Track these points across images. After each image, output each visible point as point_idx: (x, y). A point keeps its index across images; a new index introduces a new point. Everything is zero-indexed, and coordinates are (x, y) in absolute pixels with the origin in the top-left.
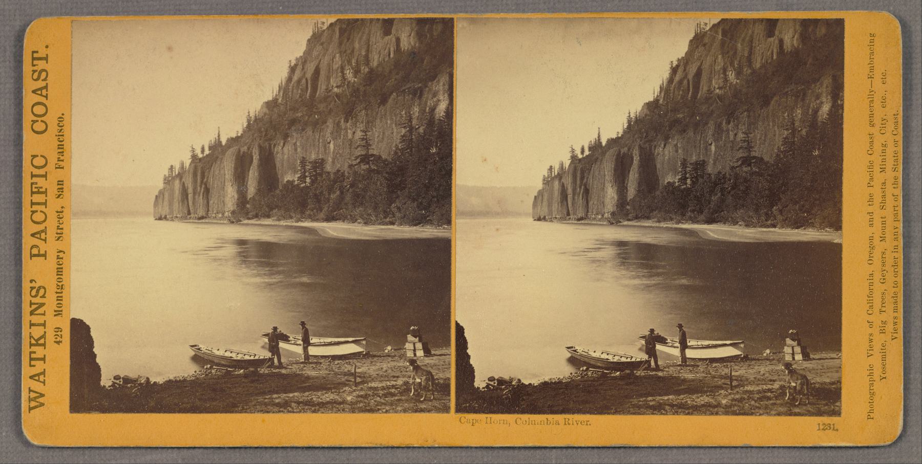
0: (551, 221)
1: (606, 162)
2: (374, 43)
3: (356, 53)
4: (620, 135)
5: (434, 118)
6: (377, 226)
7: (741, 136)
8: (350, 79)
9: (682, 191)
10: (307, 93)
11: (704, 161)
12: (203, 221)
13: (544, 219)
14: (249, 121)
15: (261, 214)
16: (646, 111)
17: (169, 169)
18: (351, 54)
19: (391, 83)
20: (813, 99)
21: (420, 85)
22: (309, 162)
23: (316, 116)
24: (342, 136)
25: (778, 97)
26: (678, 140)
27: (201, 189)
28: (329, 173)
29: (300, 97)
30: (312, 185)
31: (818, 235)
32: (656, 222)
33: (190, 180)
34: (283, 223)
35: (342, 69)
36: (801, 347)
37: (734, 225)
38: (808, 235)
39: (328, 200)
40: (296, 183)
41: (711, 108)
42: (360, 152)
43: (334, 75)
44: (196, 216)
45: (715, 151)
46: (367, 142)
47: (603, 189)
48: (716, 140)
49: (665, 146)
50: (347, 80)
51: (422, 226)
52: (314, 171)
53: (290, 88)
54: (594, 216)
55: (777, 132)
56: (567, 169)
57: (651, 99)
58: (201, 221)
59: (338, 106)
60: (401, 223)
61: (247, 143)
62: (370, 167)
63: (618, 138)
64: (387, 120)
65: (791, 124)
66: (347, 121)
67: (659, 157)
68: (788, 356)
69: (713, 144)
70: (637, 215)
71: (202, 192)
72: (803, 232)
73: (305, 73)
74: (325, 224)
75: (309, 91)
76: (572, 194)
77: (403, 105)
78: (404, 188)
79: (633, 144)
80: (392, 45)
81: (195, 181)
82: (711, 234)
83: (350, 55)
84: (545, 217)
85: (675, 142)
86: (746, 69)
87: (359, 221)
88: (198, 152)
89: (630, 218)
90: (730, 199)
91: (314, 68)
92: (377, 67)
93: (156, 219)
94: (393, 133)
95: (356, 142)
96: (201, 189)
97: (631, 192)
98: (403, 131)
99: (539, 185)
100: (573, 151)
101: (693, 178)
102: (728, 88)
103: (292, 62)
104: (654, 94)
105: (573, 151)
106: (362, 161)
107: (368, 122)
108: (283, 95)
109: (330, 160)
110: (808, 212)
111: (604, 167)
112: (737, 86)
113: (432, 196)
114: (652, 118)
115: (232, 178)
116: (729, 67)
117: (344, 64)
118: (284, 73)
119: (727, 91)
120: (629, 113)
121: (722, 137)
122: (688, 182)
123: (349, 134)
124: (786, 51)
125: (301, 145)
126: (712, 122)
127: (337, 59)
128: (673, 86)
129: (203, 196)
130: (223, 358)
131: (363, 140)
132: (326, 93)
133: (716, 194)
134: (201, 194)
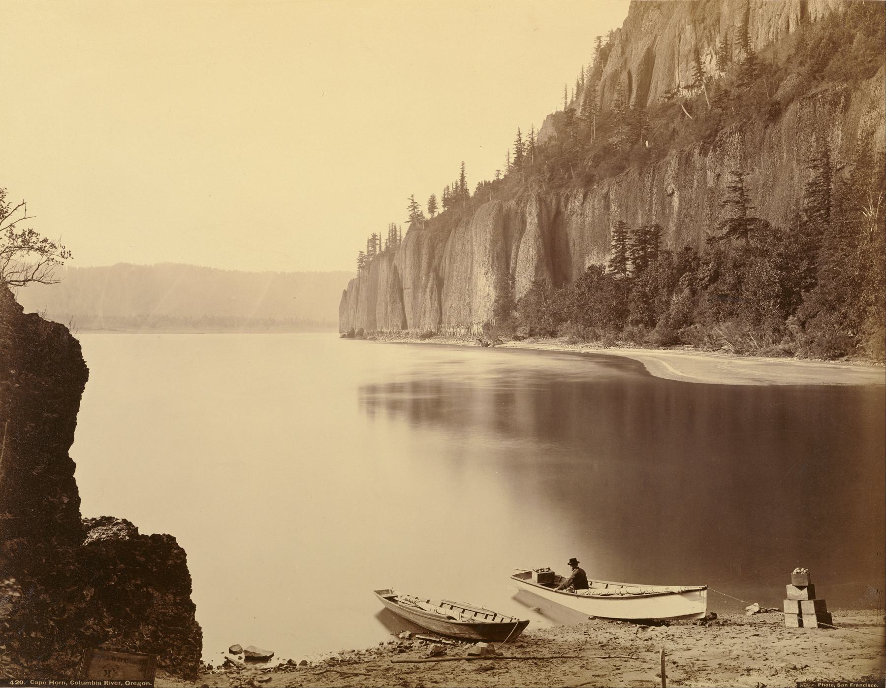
0: (374, 339)
1: (476, 228)
2: (759, 5)
3: (724, 24)
4: (501, 177)
5: (870, 150)
6: (759, 358)
7: (728, 179)
8: (712, 74)
9: (617, 286)
10: (629, 98)
11: (657, 226)
12: (431, 341)
13: (361, 335)
14: (519, 151)
15: (541, 329)
16: (552, 131)
17: (370, 241)
18: (714, 26)
19: (788, 84)
20: (864, 110)
21: (845, 85)
22: (633, 232)
23: (647, 143)
24: (695, 182)
25: (799, 106)
26: (609, 186)
27: (427, 281)
28: (669, 253)
29: (617, 106)
30: (638, 277)
31: (874, 373)
32: (568, 343)
33: (408, 263)
34: (581, 348)
35: (697, 53)
36: (815, 602)
37: (714, 351)
38: (854, 372)
39: (668, 303)
40: (607, 271)
41: (672, 126)
42: (729, 213)
43: (683, 65)
44: (418, 330)
45: (679, 208)
46: (742, 194)
47: (470, 278)
48: (681, 187)
49: (585, 197)
50: (705, 75)
51: (847, 360)
52: (642, 249)
53: (597, 88)
54: (451, 329)
55: (797, 173)
56: (402, 240)
57: (560, 107)
58: (427, 341)
59: (688, 125)
60: (807, 353)
61: (517, 192)
62: (748, 242)
63: (498, 182)
64: (781, 152)
65: (823, 156)
66: (704, 153)
67: (574, 217)
68: (792, 620)
69: (676, 194)
70: (531, 330)
71: (429, 286)
72: (846, 367)
73: (626, 61)
74: (660, 353)
75: (634, 96)
76: (411, 287)
77: (811, 124)
78: (813, 285)
79: (526, 194)
80: (792, 8)
81: (417, 265)
82: (671, 369)
83: (712, 28)
84: (362, 330)
85: (604, 191)
86: (737, 51)
87: (725, 347)
88: (424, 209)
89: (519, 334)
90: (704, 303)
91: (644, 51)
92: (764, 50)
93: (343, 336)
94: (792, 179)
95: (722, 195)
96: (427, 281)
97: (523, 283)
98: (813, 174)
99: (352, 269)
100: (414, 206)
101: (636, 258)
102: (703, 87)
103: (602, 39)
104: (566, 98)
105: (414, 206)
106: (733, 230)
107: (746, 157)
108: (585, 102)
109: (672, 227)
110: (853, 326)
111: (471, 237)
112: (722, 84)
113: (866, 302)
114: (562, 144)
115: (485, 259)
116: (706, 45)
117: (700, 44)
118: (587, 59)
119: (703, 93)
120: (519, 135)
121: (693, 180)
122: (627, 266)
123: (708, 178)
124: (813, 18)
125: (616, 198)
126: (674, 152)
127: (688, 34)
128: (601, 82)
129: (432, 292)
130: (436, 618)
131: (735, 191)
132: (666, 100)
133: (681, 291)
134: (428, 290)
